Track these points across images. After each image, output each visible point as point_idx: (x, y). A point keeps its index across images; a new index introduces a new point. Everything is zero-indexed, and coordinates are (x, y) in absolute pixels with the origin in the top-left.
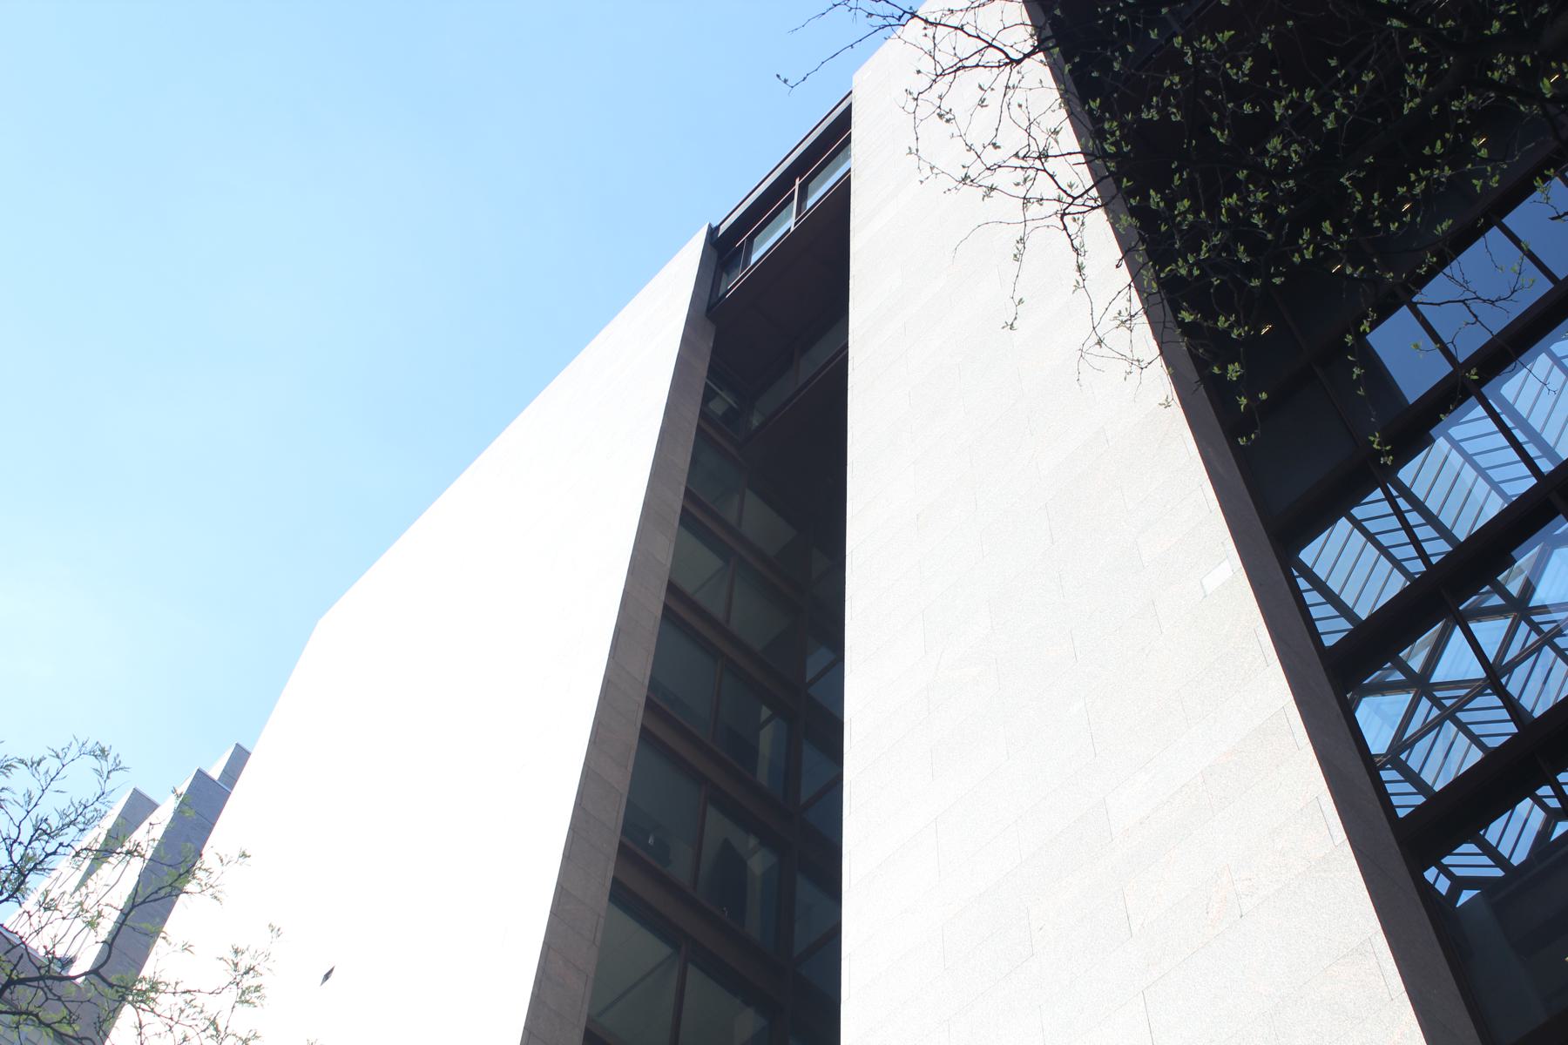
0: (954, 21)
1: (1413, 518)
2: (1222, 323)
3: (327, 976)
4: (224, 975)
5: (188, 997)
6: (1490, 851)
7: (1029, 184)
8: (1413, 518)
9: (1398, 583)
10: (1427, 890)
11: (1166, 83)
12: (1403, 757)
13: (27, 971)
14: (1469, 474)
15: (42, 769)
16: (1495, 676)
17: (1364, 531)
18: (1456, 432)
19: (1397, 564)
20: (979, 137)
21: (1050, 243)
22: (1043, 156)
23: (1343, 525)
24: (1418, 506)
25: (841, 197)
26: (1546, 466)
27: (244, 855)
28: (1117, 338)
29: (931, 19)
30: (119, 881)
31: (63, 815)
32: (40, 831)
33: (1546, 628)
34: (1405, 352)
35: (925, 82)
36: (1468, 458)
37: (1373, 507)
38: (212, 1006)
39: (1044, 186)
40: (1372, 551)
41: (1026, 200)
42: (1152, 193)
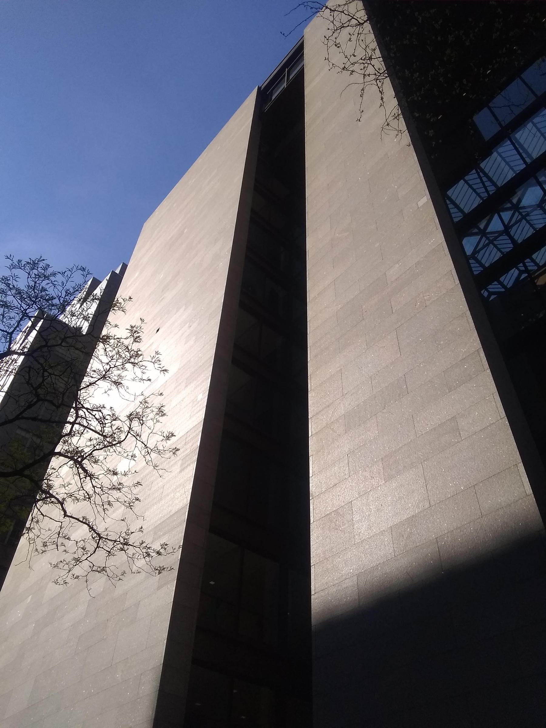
0: (340, 9)
1: (484, 179)
2: (428, 116)
3: (158, 331)
4: (127, 334)
5: (118, 340)
6: (501, 283)
7: (365, 69)
8: (484, 179)
9: (478, 201)
10: (482, 296)
11: (412, 30)
12: (476, 256)
13: (69, 334)
14: (503, 164)
15: (66, 275)
16: (507, 229)
17: (472, 188)
18: (500, 150)
19: (478, 194)
20: (349, 53)
21: (372, 90)
22: (370, 58)
23: (462, 182)
24: (486, 175)
25: (301, 75)
26: (528, 161)
27: (130, 298)
28: (394, 123)
29: (333, 9)
30: (92, 308)
31: (74, 288)
32: (68, 293)
33: (524, 214)
34: (485, 123)
35: (330, 33)
36: (503, 159)
37: (472, 176)
38: (126, 342)
39: (370, 70)
40: (470, 191)
41: (364, 75)
42: (406, 71)
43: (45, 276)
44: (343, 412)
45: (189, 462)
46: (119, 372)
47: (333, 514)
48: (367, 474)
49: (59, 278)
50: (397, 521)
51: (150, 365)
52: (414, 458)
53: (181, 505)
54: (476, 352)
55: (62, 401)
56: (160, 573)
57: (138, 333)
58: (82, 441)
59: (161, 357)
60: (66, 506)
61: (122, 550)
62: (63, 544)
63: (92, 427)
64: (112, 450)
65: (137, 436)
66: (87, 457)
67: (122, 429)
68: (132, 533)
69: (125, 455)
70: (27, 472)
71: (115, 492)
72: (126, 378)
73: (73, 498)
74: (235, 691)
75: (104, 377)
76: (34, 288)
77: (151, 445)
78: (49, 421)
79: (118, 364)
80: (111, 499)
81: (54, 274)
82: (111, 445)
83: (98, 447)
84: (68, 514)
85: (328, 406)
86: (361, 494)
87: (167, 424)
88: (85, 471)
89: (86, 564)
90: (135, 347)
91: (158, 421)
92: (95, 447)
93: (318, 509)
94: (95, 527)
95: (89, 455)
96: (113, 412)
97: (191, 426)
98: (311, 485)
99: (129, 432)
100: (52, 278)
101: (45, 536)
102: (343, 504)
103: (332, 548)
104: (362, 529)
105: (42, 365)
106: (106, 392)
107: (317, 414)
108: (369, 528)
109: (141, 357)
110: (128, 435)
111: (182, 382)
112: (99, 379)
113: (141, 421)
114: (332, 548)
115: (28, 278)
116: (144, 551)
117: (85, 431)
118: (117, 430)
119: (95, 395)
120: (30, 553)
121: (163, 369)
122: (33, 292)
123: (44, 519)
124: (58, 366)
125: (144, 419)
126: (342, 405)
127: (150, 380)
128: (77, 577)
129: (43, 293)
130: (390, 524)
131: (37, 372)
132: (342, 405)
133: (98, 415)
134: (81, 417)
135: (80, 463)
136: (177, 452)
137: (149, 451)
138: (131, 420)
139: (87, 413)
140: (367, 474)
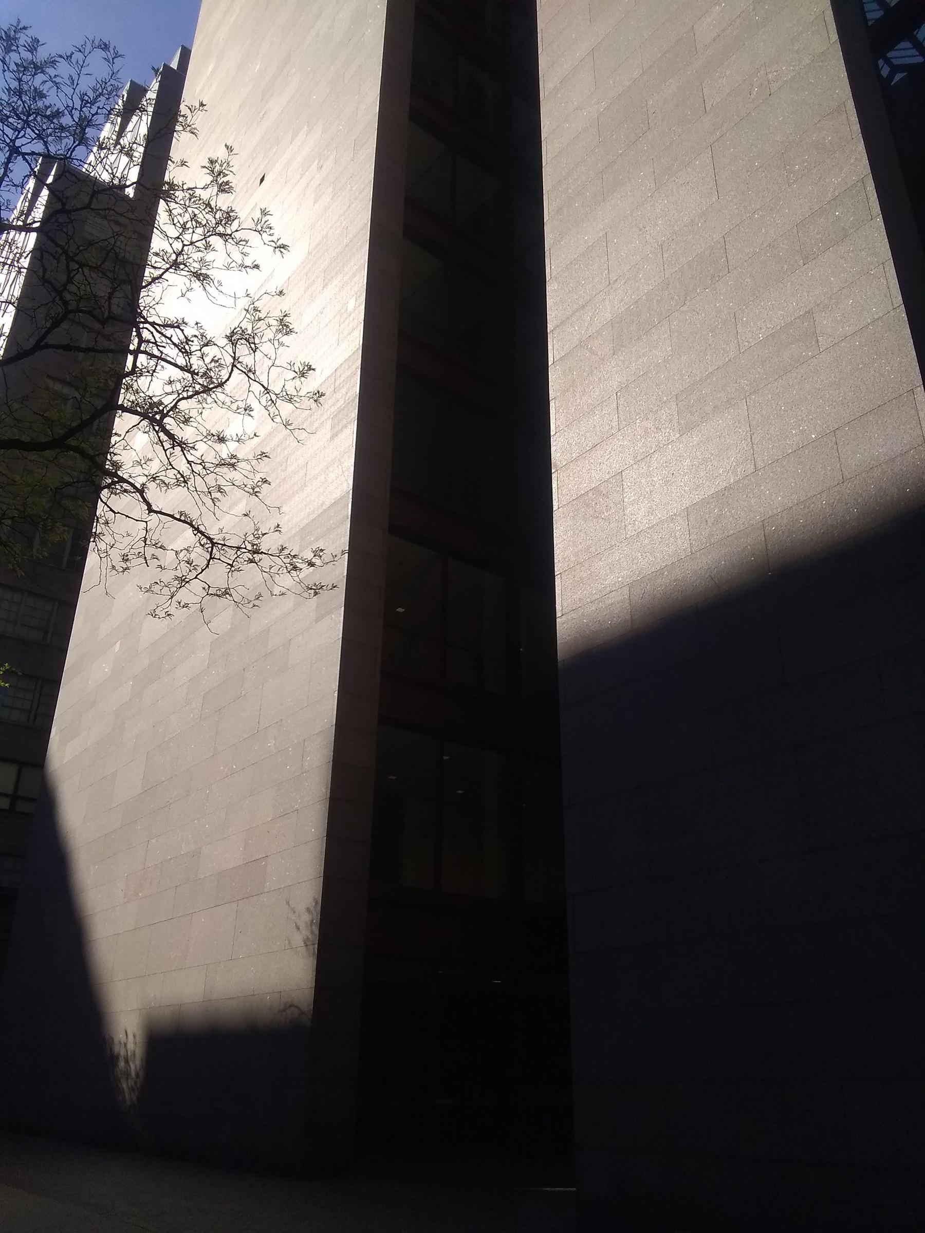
15: (74, 60)
27: (202, 105)
32: (85, 102)
38: (205, 195)
43: (36, 67)
44: (609, 316)
45: (345, 422)
46: (200, 255)
47: (590, 494)
48: (649, 424)
49: (64, 70)
50: (697, 497)
51: (254, 238)
52: (733, 390)
53: (338, 494)
54: (859, 184)
55: (110, 312)
56: (316, 594)
57: (225, 175)
58: (156, 383)
59: (272, 220)
60: (148, 495)
61: (251, 561)
62: (154, 557)
63: (168, 359)
64: (209, 400)
65: (249, 372)
66: (168, 412)
67: (223, 362)
68: (264, 535)
69: (234, 407)
70: (72, 442)
71: (225, 469)
72: (215, 264)
73: (158, 482)
74: (445, 758)
75: (175, 265)
76: (19, 93)
77: (276, 388)
78: (93, 350)
79: (196, 237)
80: (222, 482)
81: (53, 63)
82: (207, 390)
83: (185, 394)
84: (154, 508)
85: (583, 307)
86: (639, 458)
87: (295, 349)
88: (171, 436)
89: (196, 586)
90: (223, 202)
91: (281, 344)
92: (179, 394)
93: (564, 488)
94: (202, 528)
95: (171, 409)
96: (202, 331)
97: (341, 359)
98: (553, 449)
99: (234, 366)
100: (51, 71)
101: (123, 545)
102: (608, 477)
103: (589, 547)
104: (639, 514)
105: (62, 247)
106: (183, 295)
107: (563, 323)
108: (651, 511)
109: (236, 221)
110: (232, 370)
111: (317, 277)
112: (167, 270)
113: (253, 346)
114: (589, 547)
115: (4, 71)
116: (288, 560)
117: (159, 367)
118: (213, 364)
119: (166, 299)
120: (104, 573)
121: (278, 244)
122: (20, 102)
123: (118, 520)
124: (95, 260)
125: (257, 341)
126: (607, 303)
127: (257, 267)
128: (186, 606)
129: (40, 104)
130: (687, 503)
131: (54, 258)
132: (607, 303)
133: (176, 335)
134: (148, 342)
135: (160, 423)
136: (321, 399)
137: (274, 399)
138: (234, 344)
139: (157, 335)
140: (649, 424)
